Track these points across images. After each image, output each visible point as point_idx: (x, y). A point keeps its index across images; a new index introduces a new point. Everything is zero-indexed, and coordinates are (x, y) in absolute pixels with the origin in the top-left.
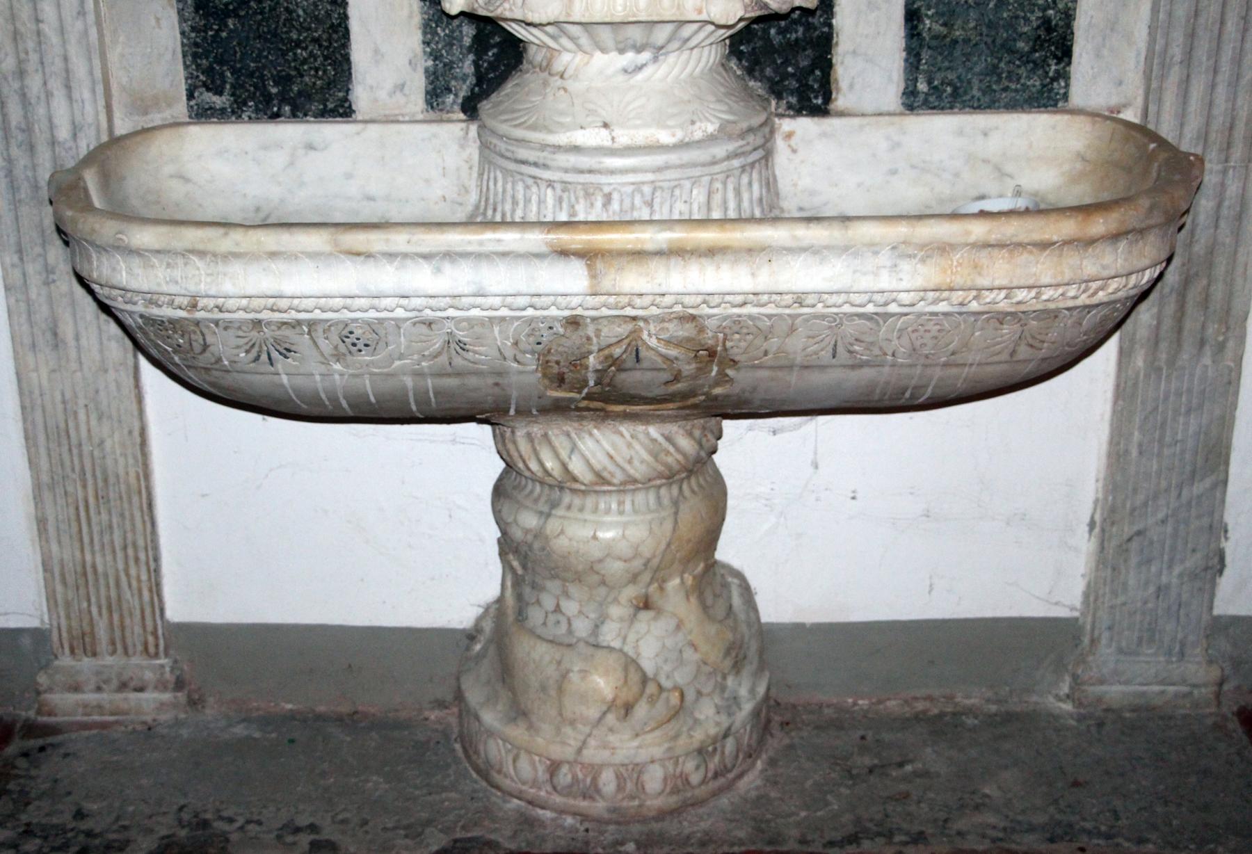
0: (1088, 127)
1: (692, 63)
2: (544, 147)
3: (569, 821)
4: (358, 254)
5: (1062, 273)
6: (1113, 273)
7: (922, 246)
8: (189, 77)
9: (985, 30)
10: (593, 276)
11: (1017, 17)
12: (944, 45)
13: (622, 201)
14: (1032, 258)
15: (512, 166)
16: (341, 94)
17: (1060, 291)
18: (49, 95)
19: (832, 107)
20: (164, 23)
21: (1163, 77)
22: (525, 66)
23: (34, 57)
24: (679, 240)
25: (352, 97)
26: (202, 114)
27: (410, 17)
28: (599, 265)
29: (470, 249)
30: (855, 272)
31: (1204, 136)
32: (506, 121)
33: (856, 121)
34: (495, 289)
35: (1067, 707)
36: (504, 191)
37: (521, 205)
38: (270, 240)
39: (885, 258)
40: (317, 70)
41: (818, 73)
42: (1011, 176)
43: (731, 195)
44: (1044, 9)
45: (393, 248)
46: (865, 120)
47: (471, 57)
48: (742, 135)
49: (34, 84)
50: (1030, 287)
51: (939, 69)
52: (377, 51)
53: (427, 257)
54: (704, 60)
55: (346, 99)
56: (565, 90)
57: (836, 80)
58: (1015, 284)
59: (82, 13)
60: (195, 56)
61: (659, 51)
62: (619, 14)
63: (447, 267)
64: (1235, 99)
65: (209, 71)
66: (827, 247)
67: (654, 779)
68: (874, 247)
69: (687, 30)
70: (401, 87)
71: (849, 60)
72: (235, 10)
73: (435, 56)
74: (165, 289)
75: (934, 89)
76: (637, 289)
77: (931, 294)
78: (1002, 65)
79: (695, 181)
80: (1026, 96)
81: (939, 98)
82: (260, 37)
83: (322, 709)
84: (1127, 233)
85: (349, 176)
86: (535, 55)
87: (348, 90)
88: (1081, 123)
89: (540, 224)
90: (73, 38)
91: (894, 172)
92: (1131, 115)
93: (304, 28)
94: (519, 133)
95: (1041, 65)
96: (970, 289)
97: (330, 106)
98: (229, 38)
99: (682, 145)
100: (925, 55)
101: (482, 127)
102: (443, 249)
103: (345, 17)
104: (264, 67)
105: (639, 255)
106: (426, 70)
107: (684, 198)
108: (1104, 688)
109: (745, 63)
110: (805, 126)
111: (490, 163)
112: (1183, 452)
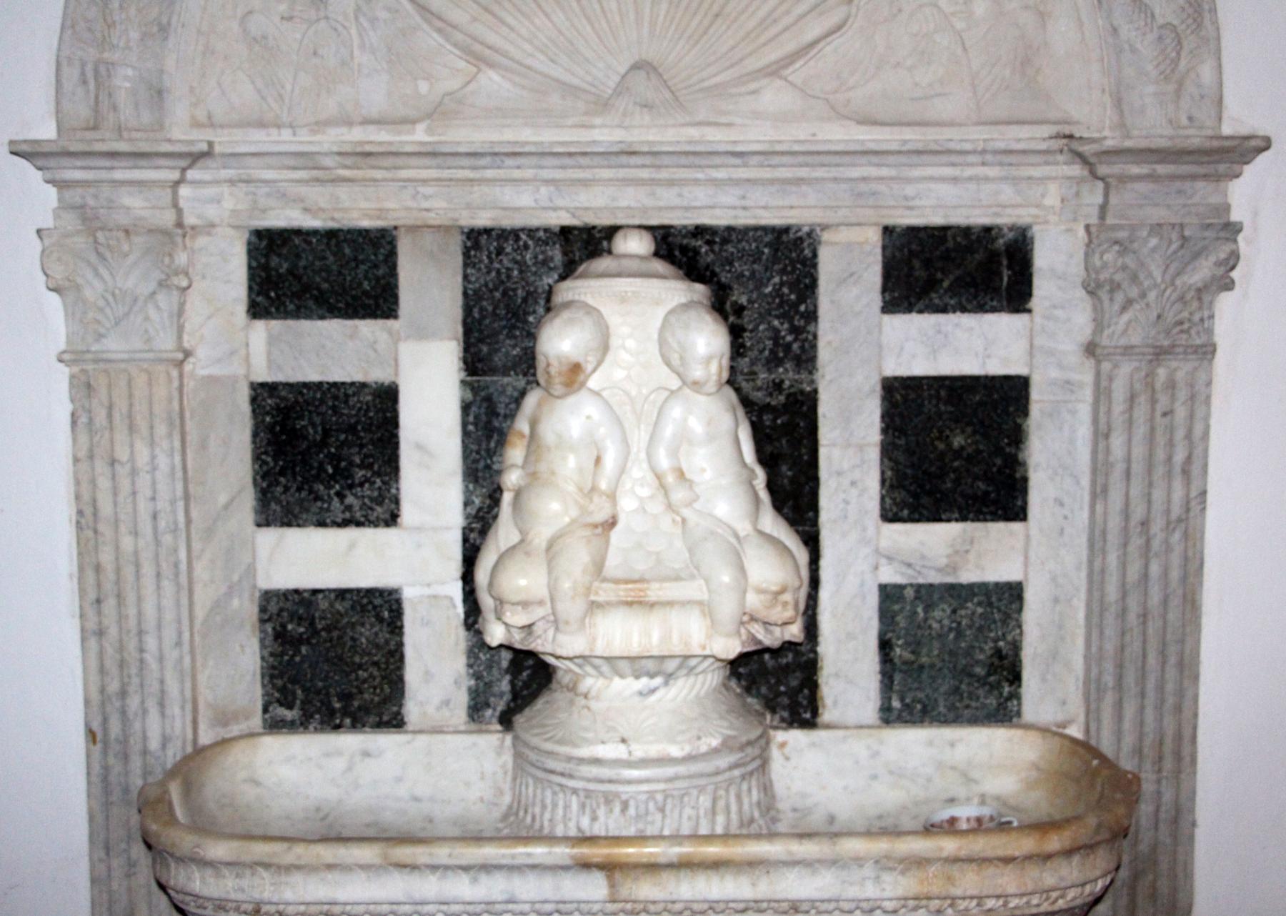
0: (1040, 741)
1: (698, 686)
2: (570, 759)
4: (405, 866)
5: (1025, 884)
6: (1069, 884)
7: (902, 861)
9: (947, 657)
10: (612, 886)
11: (973, 647)
12: (914, 670)
13: (637, 808)
14: (998, 871)
15: (540, 774)
16: (395, 709)
17: (1025, 899)
18: (145, 712)
19: (819, 720)
20: (248, 650)
21: (1100, 700)
22: (554, 685)
23: (135, 681)
24: (688, 854)
25: (405, 711)
26: (275, 726)
27: (457, 644)
28: (618, 875)
29: (504, 862)
30: (844, 882)
31: (1138, 751)
32: (537, 735)
34: (524, 897)
36: (535, 796)
37: (549, 809)
38: (327, 853)
39: (869, 870)
40: (375, 688)
41: (806, 691)
42: (976, 782)
43: (733, 800)
44: (996, 641)
45: (436, 861)
46: (848, 732)
47: (508, 677)
48: (742, 748)
49: (133, 703)
50: (998, 897)
51: (910, 689)
52: (427, 673)
53: (466, 868)
54: (708, 683)
55: (399, 713)
56: (589, 708)
57: (822, 698)
58: (985, 893)
59: (179, 644)
60: (272, 677)
61: (669, 677)
62: (635, 650)
63: (483, 878)
64: (1161, 720)
65: (282, 690)
66: (819, 861)
68: (859, 861)
69: (693, 662)
70: (446, 703)
71: (832, 681)
72: (308, 639)
73: (477, 677)
74: (233, 896)
75: (907, 707)
76: (651, 897)
78: (963, 687)
79: (702, 789)
80: (985, 712)
82: (327, 660)
84: (1079, 849)
85: (399, 780)
86: (562, 677)
87: (401, 706)
88: (1033, 736)
89: (566, 839)
90: (169, 665)
91: (874, 777)
92: (1075, 732)
93: (366, 653)
94: (549, 746)
95: (996, 687)
96: (945, 898)
97: (385, 718)
98: (302, 662)
99: (689, 758)
100: (898, 677)
101: (516, 738)
102: (480, 861)
103: (400, 645)
104: (330, 686)
105: (653, 867)
106: (470, 689)
107: (692, 803)
109: (744, 683)
110: (796, 737)
111: (522, 769)
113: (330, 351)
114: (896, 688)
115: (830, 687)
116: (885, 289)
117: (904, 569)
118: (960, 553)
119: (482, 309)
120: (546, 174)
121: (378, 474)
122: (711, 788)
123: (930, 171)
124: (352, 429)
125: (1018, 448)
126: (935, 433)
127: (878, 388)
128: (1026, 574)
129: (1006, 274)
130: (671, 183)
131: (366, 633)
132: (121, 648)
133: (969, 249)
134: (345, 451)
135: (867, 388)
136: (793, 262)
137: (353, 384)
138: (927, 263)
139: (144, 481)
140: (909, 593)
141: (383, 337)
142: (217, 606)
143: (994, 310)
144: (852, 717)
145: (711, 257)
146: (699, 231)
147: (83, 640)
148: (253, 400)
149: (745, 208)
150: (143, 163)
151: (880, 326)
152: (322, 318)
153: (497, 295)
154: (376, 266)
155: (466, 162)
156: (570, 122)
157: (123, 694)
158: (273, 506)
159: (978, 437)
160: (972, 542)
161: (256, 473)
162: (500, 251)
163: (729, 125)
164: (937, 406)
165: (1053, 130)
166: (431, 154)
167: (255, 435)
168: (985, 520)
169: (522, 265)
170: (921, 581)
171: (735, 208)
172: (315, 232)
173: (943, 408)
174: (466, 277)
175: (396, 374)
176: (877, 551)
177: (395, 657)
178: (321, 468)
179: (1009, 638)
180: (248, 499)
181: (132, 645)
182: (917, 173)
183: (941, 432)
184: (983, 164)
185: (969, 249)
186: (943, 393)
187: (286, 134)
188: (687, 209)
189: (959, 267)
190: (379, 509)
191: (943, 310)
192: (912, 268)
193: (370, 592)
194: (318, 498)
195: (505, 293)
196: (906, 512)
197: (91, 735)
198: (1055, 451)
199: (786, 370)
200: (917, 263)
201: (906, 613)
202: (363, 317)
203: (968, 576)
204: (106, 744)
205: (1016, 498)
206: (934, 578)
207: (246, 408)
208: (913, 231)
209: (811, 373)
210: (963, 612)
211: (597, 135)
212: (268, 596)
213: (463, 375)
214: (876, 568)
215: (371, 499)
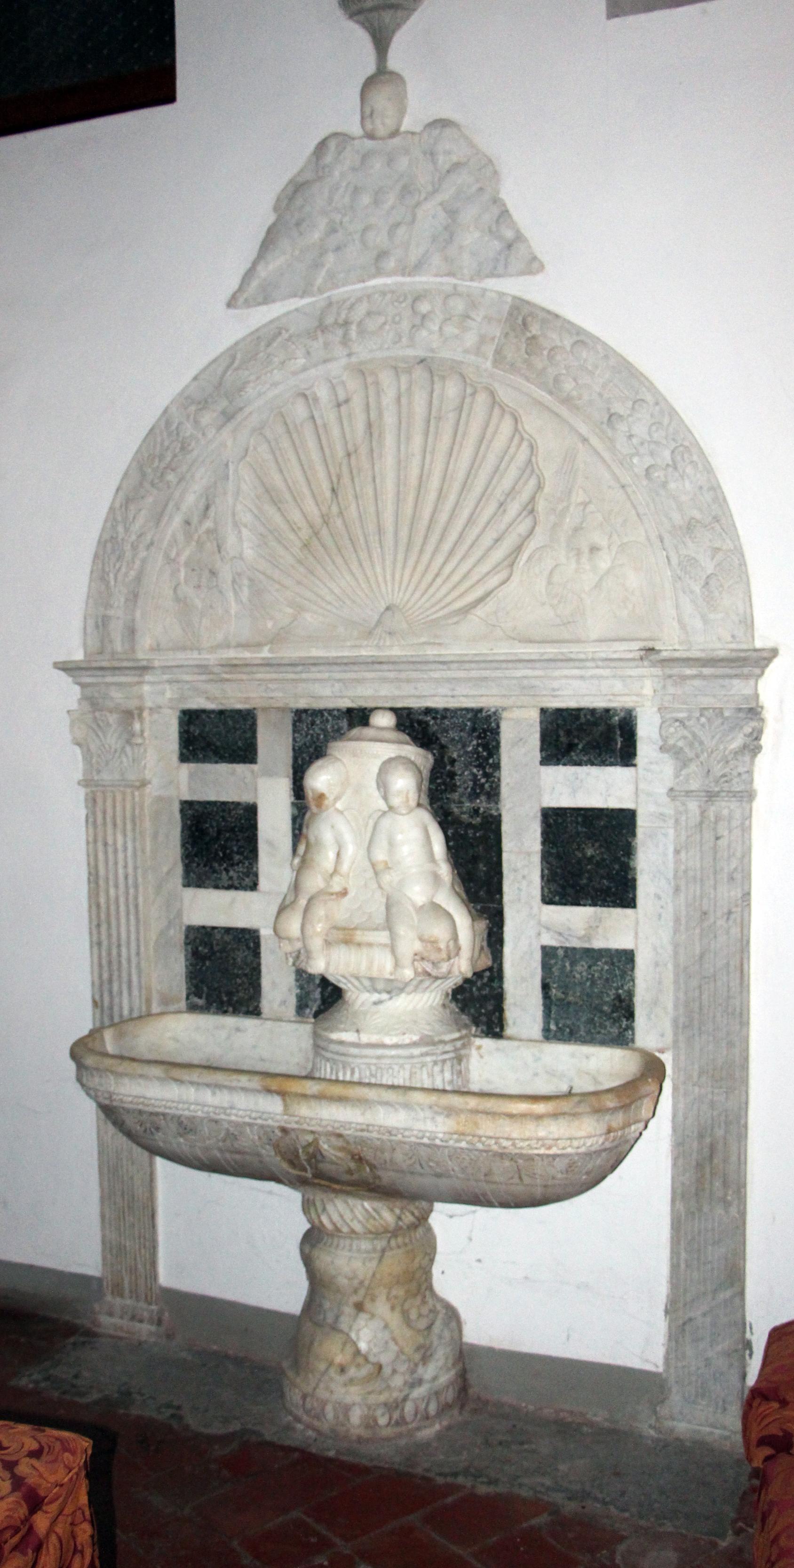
3: (310, 1433)
8: (188, 988)
10: (286, 1106)
26: (193, 1008)
33: (516, 1043)
35: (652, 1432)
44: (617, 989)
47: (319, 990)
60: (191, 978)
65: (196, 986)
67: (356, 1416)
73: (301, 987)
75: (560, 1029)
77: (455, 1136)
81: (563, 1034)
83: (231, 1352)
85: (254, 1047)
87: (259, 1002)
103: (259, 964)
108: (675, 1423)
110: (487, 1043)
112: (713, 1269)
113: (221, 782)
114: (553, 1016)
115: (511, 1013)
116: (542, 750)
117: (556, 936)
118: (592, 928)
119: (303, 759)
120: (338, 676)
121: (246, 858)
122: (408, 1067)
123: (566, 672)
124: (232, 830)
125: (629, 858)
126: (575, 846)
127: (539, 814)
128: (636, 945)
129: (619, 740)
130: (408, 681)
131: (240, 955)
132: (109, 954)
133: (595, 724)
134: (229, 844)
135: (532, 814)
136: (485, 731)
137: (233, 803)
138: (568, 733)
139: (121, 856)
140: (561, 953)
141: (248, 775)
142: (162, 933)
143: (612, 764)
144: (525, 1033)
145: (436, 728)
146: (428, 711)
147: (91, 947)
148: (182, 811)
149: (453, 697)
150: (117, 672)
151: (539, 773)
152: (216, 762)
153: (311, 750)
154: (245, 732)
155: (289, 669)
156: (349, 644)
157: (110, 981)
158: (192, 874)
159: (603, 850)
160: (600, 921)
161: (183, 855)
162: (313, 723)
163: (440, 644)
164: (576, 828)
165: (641, 644)
166: (267, 664)
167: (182, 832)
168: (609, 906)
169: (324, 731)
170: (568, 945)
171: (446, 696)
172: (213, 712)
173: (580, 829)
174: (294, 739)
175: (256, 797)
176: (539, 923)
177: (255, 972)
178: (216, 854)
179: (626, 988)
180: (179, 870)
181: (114, 952)
182: (557, 673)
183: (579, 845)
184: (597, 667)
185: (595, 724)
186: (580, 819)
187: (195, 655)
188: (418, 697)
189: (590, 735)
190: (247, 880)
191: (579, 764)
192: (558, 736)
193: (243, 931)
194: (214, 871)
195: (316, 749)
196: (557, 898)
197: (95, 1003)
198: (653, 861)
199: (481, 802)
200: (561, 733)
201: (558, 966)
202: (239, 762)
203: (598, 944)
204: (102, 1007)
205: (628, 892)
206: (575, 943)
207: (178, 816)
208: (559, 711)
209: (497, 803)
210: (595, 968)
211: (364, 653)
212: (190, 929)
213: (293, 799)
214: (539, 934)
215: (243, 873)
